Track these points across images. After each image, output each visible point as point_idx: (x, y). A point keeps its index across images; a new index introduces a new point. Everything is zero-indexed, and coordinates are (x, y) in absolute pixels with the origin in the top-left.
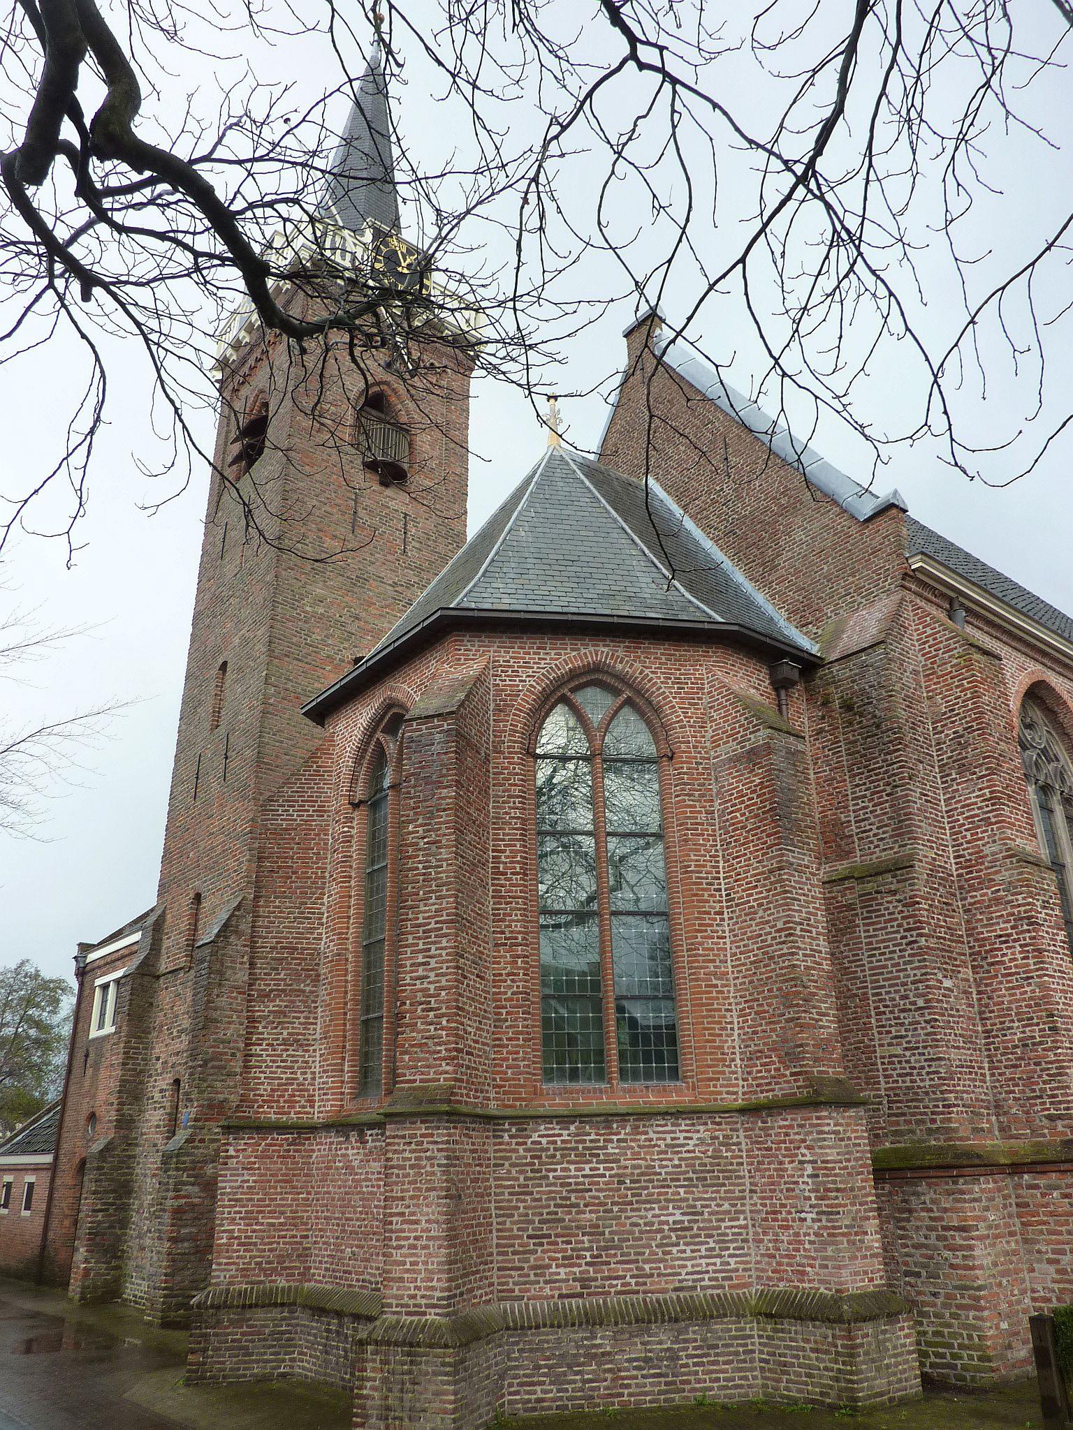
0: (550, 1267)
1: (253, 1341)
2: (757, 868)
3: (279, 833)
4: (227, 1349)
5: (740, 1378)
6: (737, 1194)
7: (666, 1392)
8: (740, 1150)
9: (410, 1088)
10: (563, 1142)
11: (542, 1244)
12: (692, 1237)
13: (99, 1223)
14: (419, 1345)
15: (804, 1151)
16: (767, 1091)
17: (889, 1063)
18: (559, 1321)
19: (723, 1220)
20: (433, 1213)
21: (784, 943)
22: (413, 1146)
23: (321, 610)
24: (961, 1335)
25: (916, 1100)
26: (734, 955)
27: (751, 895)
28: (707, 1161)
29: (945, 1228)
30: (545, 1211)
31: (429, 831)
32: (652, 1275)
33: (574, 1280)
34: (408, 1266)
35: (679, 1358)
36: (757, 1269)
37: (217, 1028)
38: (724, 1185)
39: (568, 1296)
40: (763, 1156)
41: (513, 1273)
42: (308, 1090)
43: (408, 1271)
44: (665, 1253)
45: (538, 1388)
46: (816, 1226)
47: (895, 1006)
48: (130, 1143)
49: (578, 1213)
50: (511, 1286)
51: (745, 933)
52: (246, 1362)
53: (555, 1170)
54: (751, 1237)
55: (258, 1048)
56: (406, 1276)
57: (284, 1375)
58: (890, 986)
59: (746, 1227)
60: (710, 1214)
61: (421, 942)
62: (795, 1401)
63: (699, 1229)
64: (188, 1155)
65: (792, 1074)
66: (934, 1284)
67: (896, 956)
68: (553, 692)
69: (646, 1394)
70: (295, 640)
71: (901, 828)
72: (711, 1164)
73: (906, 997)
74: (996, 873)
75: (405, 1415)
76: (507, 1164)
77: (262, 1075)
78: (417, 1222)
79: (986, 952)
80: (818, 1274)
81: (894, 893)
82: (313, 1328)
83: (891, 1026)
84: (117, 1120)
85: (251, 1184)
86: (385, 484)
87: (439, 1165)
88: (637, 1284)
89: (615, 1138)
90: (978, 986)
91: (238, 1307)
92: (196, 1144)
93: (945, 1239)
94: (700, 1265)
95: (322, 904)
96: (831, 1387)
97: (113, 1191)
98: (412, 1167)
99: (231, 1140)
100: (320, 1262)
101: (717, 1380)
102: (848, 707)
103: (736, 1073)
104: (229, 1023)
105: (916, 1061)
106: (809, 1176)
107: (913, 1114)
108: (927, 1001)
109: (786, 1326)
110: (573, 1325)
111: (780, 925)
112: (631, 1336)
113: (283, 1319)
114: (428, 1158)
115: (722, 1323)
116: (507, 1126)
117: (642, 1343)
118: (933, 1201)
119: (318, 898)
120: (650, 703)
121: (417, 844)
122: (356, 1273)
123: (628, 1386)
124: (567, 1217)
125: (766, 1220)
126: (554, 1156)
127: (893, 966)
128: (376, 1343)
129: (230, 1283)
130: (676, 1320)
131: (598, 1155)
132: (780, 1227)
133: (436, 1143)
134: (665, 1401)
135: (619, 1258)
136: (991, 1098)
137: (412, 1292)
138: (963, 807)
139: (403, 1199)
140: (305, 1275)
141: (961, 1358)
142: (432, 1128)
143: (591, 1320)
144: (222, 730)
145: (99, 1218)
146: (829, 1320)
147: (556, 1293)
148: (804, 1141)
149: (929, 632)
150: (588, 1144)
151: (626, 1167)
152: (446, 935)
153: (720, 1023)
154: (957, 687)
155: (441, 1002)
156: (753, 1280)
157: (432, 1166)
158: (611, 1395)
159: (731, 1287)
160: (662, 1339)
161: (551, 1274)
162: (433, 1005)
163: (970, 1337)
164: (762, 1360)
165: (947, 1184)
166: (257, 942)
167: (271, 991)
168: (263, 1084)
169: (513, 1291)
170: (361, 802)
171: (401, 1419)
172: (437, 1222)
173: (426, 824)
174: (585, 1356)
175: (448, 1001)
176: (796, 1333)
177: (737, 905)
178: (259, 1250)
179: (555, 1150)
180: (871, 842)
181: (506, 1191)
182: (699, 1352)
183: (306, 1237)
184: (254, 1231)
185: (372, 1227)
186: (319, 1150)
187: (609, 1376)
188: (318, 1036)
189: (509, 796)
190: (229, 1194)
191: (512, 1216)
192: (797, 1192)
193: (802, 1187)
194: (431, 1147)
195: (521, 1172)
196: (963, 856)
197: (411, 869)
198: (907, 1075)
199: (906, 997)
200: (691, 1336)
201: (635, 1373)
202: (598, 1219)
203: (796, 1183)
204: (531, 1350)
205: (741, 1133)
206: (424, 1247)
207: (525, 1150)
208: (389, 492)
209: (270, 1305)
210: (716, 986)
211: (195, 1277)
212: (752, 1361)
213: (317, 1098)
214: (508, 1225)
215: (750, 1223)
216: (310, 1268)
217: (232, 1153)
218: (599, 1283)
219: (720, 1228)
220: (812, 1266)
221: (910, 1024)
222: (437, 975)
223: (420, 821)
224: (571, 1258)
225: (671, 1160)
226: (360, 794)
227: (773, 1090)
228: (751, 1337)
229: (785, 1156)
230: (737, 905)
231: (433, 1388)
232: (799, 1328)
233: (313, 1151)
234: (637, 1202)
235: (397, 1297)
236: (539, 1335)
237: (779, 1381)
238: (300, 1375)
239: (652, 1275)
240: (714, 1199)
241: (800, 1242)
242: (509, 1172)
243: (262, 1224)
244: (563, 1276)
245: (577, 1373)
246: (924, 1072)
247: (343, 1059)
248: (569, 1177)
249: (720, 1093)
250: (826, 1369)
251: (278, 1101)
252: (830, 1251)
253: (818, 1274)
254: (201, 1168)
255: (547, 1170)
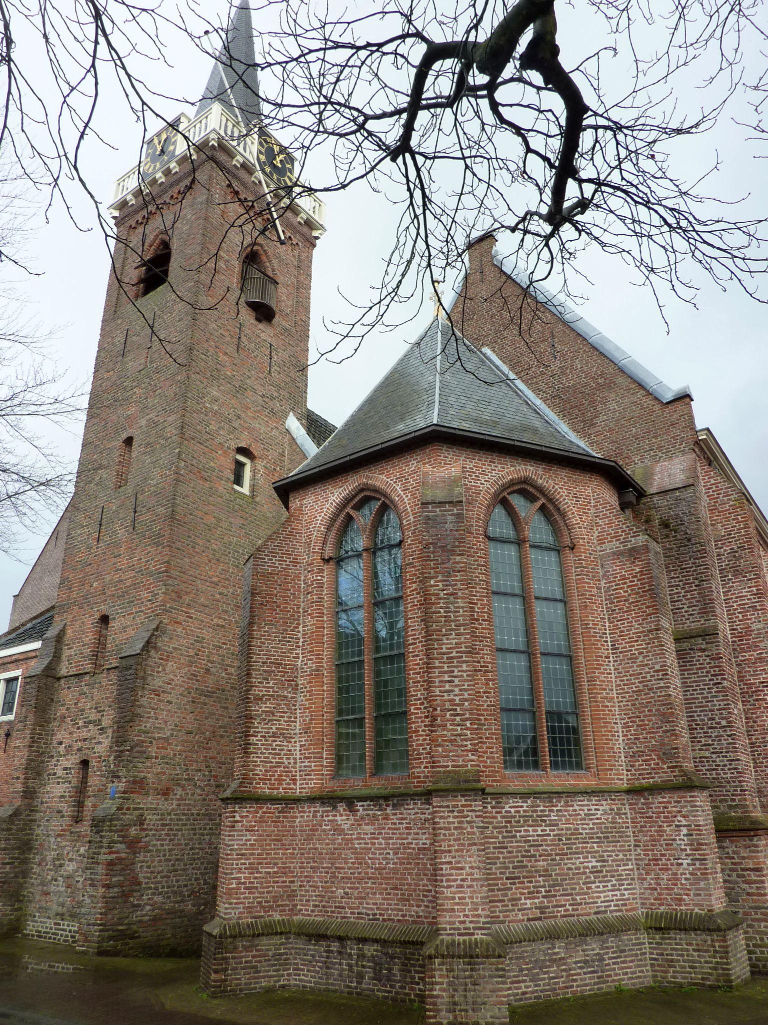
0: (520, 899)
1: (260, 962)
2: (638, 628)
3: (267, 576)
4: (242, 968)
5: (640, 972)
6: (627, 848)
7: (598, 983)
8: (627, 818)
9: (445, 772)
10: (524, 811)
11: (514, 884)
12: (603, 877)
13: (7, 873)
14: (477, 957)
15: (679, 818)
16: (648, 778)
17: (700, 762)
18: (532, 937)
19: (619, 866)
20: (475, 862)
21: (661, 679)
22: (456, 814)
23: (216, 408)
24: (755, 938)
25: (721, 787)
26: (617, 686)
27: (633, 646)
28: (609, 825)
29: (742, 870)
30: (516, 860)
31: (447, 585)
32: (581, 904)
33: (536, 908)
34: (457, 900)
35: (604, 960)
36: (641, 898)
37: (141, 721)
38: (619, 841)
39: (533, 920)
40: (646, 822)
41: (498, 904)
42: (291, 772)
43: (457, 904)
44: (588, 888)
45: (523, 985)
46: (691, 868)
47: (703, 724)
48: (32, 810)
49: (536, 861)
50: (498, 913)
51: (628, 672)
52: (255, 978)
53: (520, 831)
54: (636, 877)
55: (255, 739)
56: (456, 907)
57: (283, 986)
58: (701, 711)
59: (632, 870)
60: (613, 861)
61: (445, 666)
62: (681, 986)
63: (607, 871)
64: (118, 819)
65: (669, 767)
66: (735, 906)
67: (705, 692)
68: (499, 495)
69: (586, 985)
70: (198, 427)
71: (706, 608)
72: (611, 828)
73: (713, 719)
74: (760, 642)
75: (468, 1007)
76: (491, 827)
77: (258, 760)
78: (462, 868)
79: (752, 692)
80: (693, 900)
81: (704, 650)
82: (309, 950)
83: (701, 737)
84: (23, 791)
85: (252, 842)
86: (259, 320)
87: (477, 827)
88: (573, 910)
89: (555, 809)
90: (746, 713)
91: (249, 936)
92: (124, 811)
93: (744, 876)
94: (608, 896)
95: (299, 632)
96: (711, 974)
97: (18, 848)
98: (455, 828)
99: (237, 809)
100: (308, 901)
101: (626, 973)
102: (665, 525)
103: (621, 766)
104: (149, 718)
105: (720, 761)
106: (684, 835)
107: (717, 796)
108: (728, 722)
109: (672, 935)
110: (542, 939)
111: (657, 667)
112: (576, 946)
113: (282, 944)
114: (468, 822)
115: (627, 935)
116: (489, 800)
117: (583, 951)
118: (734, 852)
119: (295, 627)
120: (559, 509)
121: (438, 594)
122: (350, 908)
123: (575, 980)
124: (529, 864)
125: (649, 865)
126: (519, 821)
127: (702, 698)
128: (443, 956)
129: (239, 918)
130: (602, 934)
131: (545, 821)
132: (660, 869)
133: (474, 811)
134: (598, 989)
135: (561, 892)
136: (755, 786)
137: (462, 919)
138: (737, 597)
139: (450, 851)
140: (293, 911)
141: (755, 953)
142: (471, 800)
143: (552, 935)
144: (129, 489)
145: (7, 870)
146: (709, 930)
147: (526, 918)
148: (680, 812)
149: (713, 481)
150: (539, 813)
151: (562, 829)
152: (465, 662)
153: (611, 731)
154: (733, 520)
155: (466, 710)
156: (639, 905)
157: (472, 827)
158: (566, 987)
159: (627, 910)
160: (593, 947)
161: (522, 904)
162: (459, 711)
163: (762, 939)
164: (651, 959)
165: (745, 841)
166: (252, 658)
167: (264, 695)
168: (259, 766)
169: (499, 917)
170: (331, 558)
171: (466, 1011)
172: (479, 868)
173: (444, 581)
174: (550, 960)
175: (471, 709)
176: (681, 939)
177: (621, 652)
178: (259, 893)
179: (520, 817)
180: (684, 616)
181: (491, 846)
182: (615, 955)
183: (293, 882)
184: (255, 878)
185: (367, 873)
186: (302, 817)
187: (564, 974)
188: (297, 731)
189: (478, 565)
190: (237, 849)
191: (495, 864)
192: (675, 845)
193: (679, 842)
194: (470, 814)
195: (499, 833)
196: (736, 629)
197: (434, 612)
198: (713, 770)
199: (713, 719)
200: (610, 944)
201: (579, 971)
202: (548, 865)
203: (675, 840)
204: (517, 958)
205: (627, 807)
206: (469, 887)
207: (501, 817)
208: (261, 326)
209: (272, 934)
210: (607, 706)
211: (121, 915)
212: (645, 960)
213: (298, 778)
214: (494, 870)
215: (635, 867)
216: (297, 905)
217: (237, 818)
218: (551, 910)
219: (618, 871)
220: (687, 895)
221: (716, 737)
222: (461, 690)
223: (440, 578)
224: (533, 892)
225: (588, 824)
226: (329, 552)
227: (653, 778)
228: (644, 944)
229: (663, 822)
230: (621, 652)
231: (491, 986)
232: (683, 936)
233: (296, 817)
234: (570, 853)
235: (449, 923)
236: (521, 947)
237: (667, 972)
238: (298, 986)
239: (581, 904)
240: (614, 851)
241: (677, 879)
242: (492, 832)
243: (261, 873)
244: (529, 906)
245: (545, 973)
246: (726, 768)
247: (323, 749)
248: (529, 836)
249: (613, 779)
250: (706, 962)
251: (270, 780)
252: (702, 885)
253: (693, 900)
254: (128, 830)
255: (516, 831)
